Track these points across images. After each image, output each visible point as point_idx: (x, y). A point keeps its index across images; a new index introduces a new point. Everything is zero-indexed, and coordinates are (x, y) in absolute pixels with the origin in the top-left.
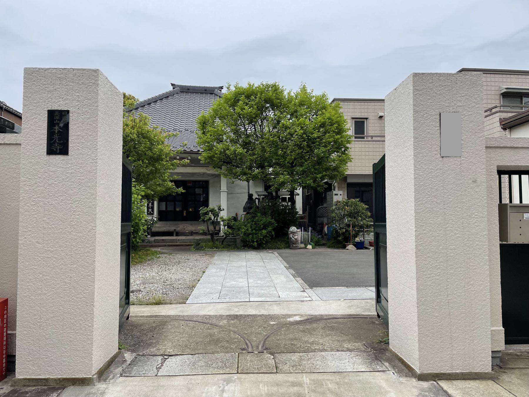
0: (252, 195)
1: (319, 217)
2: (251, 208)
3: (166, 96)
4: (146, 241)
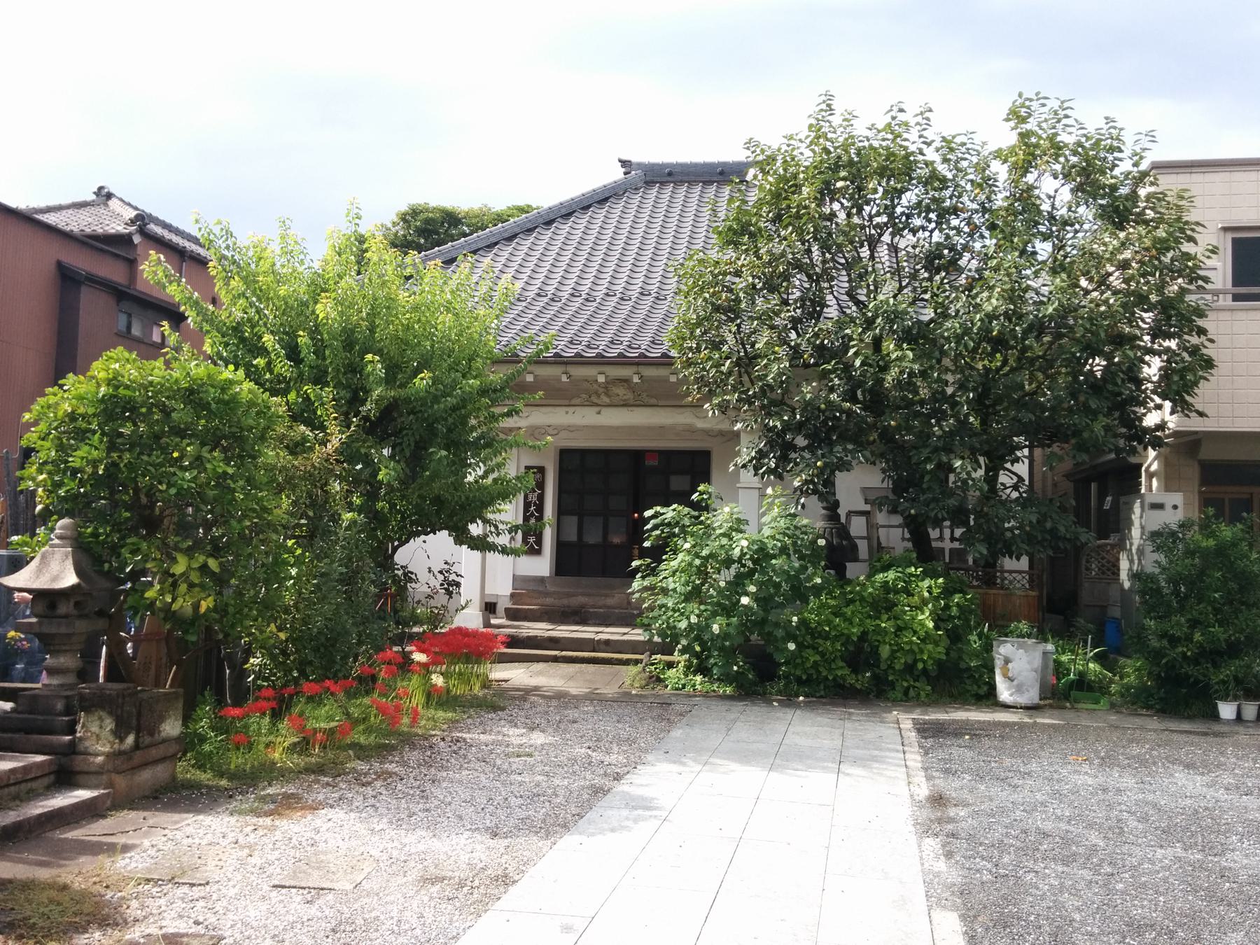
3: (603, 198)
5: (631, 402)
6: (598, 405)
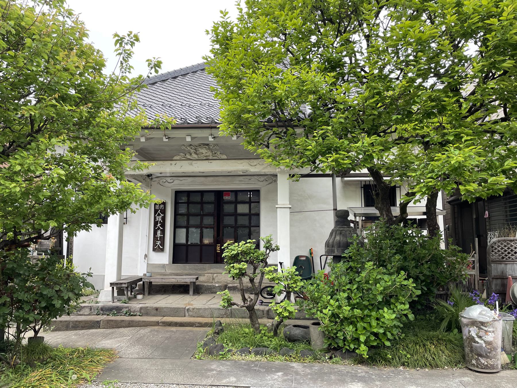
0: (346, 213)
1: (494, 262)
2: (347, 245)
4: (125, 310)
5: (211, 158)
6: (190, 160)
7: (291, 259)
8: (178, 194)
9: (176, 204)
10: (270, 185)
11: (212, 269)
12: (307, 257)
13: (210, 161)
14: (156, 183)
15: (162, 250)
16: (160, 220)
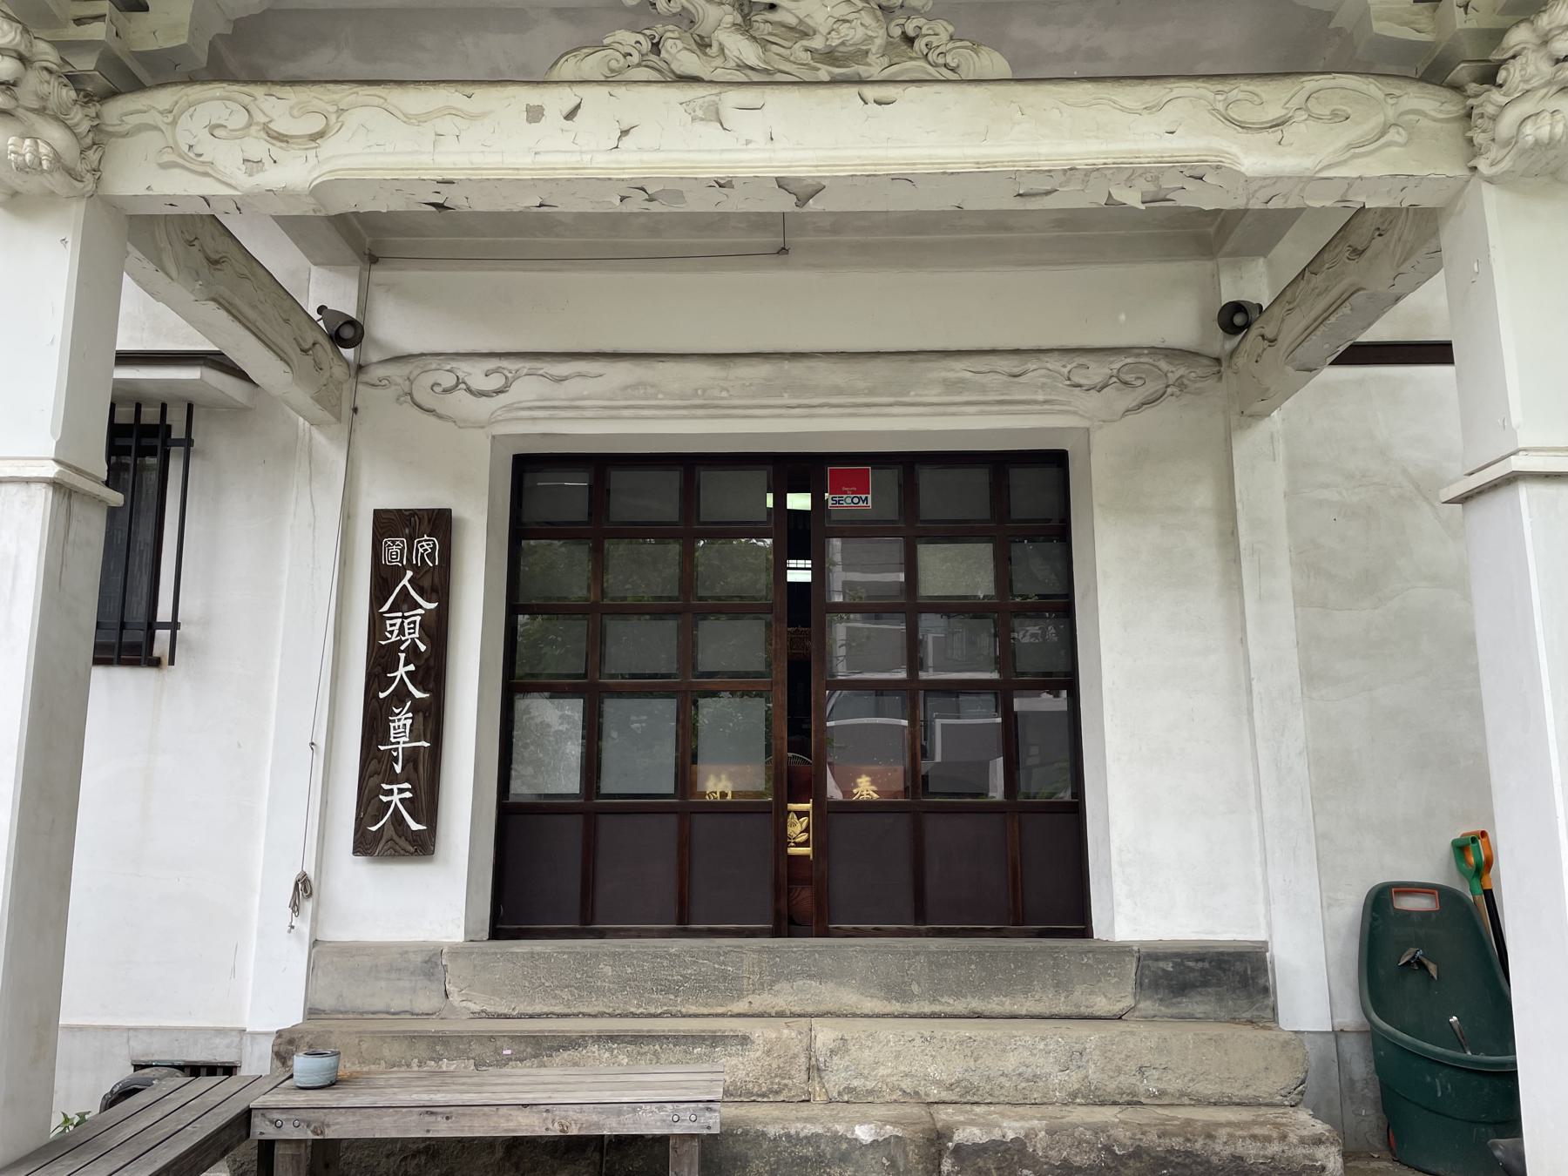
7: (1328, 904)
8: (529, 469)
9: (522, 529)
10: (1148, 414)
11: (783, 986)
12: (1445, 895)
13: (871, 92)
14: (391, 393)
15: (422, 846)
16: (412, 635)
